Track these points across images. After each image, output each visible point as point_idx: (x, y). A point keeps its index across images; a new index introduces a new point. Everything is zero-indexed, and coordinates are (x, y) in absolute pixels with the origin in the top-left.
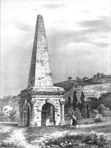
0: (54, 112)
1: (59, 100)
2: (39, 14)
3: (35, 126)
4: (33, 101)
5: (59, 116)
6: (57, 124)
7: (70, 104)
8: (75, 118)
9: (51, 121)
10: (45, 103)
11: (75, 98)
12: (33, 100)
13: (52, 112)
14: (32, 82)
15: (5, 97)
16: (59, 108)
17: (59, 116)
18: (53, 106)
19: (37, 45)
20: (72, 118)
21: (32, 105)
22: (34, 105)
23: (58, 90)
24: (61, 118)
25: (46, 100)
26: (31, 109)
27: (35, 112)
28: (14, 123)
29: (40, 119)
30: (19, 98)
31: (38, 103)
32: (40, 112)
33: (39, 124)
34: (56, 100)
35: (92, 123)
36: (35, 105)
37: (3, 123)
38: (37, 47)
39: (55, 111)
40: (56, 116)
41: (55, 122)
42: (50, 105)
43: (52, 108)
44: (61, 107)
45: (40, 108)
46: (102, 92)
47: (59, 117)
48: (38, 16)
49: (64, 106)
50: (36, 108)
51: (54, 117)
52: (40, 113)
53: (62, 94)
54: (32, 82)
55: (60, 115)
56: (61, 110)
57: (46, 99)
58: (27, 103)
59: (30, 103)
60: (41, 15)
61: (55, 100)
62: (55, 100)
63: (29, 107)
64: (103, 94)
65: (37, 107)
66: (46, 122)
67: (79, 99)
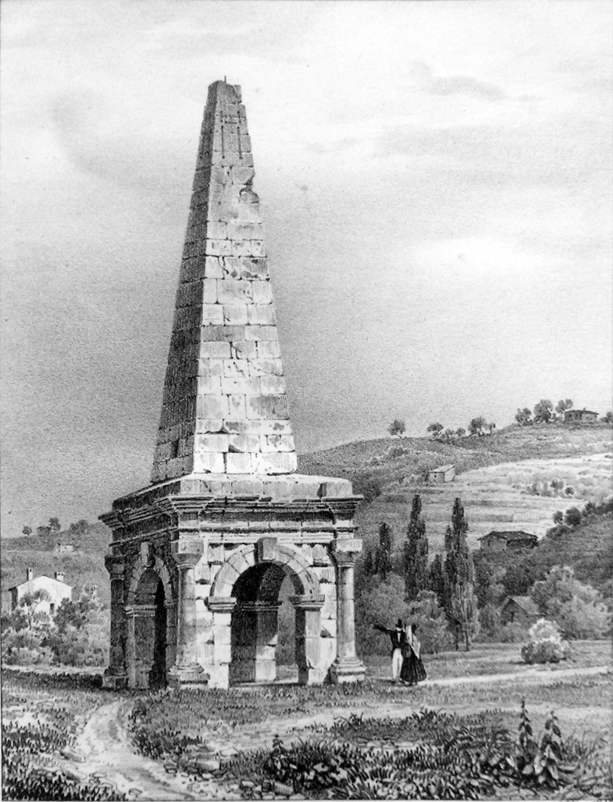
0: (300, 615)
1: (330, 547)
2: (223, 80)
3: (201, 686)
6: (316, 677)
7: (416, 519)
8: (416, 645)
9: (280, 660)
10: (294, 611)
11: (417, 530)
12: (184, 543)
13: (286, 612)
14: (176, 446)
15: (26, 531)
16: (328, 589)
17: (324, 635)
18: (295, 576)
20: (403, 645)
21: (178, 576)
22: (190, 573)
23: (320, 494)
24: (341, 642)
25: (258, 548)
26: (175, 595)
27: (196, 612)
28: (69, 670)
29: (224, 651)
30: (106, 538)
32: (227, 611)
33: (220, 679)
36: (193, 575)
37: (175, 660)
39: (305, 609)
40: (311, 636)
41: (304, 670)
42: (278, 571)
43: (286, 590)
44: (339, 583)
45: (225, 592)
46: (565, 505)
47: (327, 640)
48: (213, 89)
49: (355, 576)
50: (203, 591)
51: (301, 642)
52: (227, 618)
53: (349, 516)
54: (176, 446)
57: (254, 538)
58: (153, 564)
59: (171, 563)
60: (228, 82)
61: (300, 545)
63: (161, 586)
64: (568, 512)
66: (255, 659)
67: (436, 540)
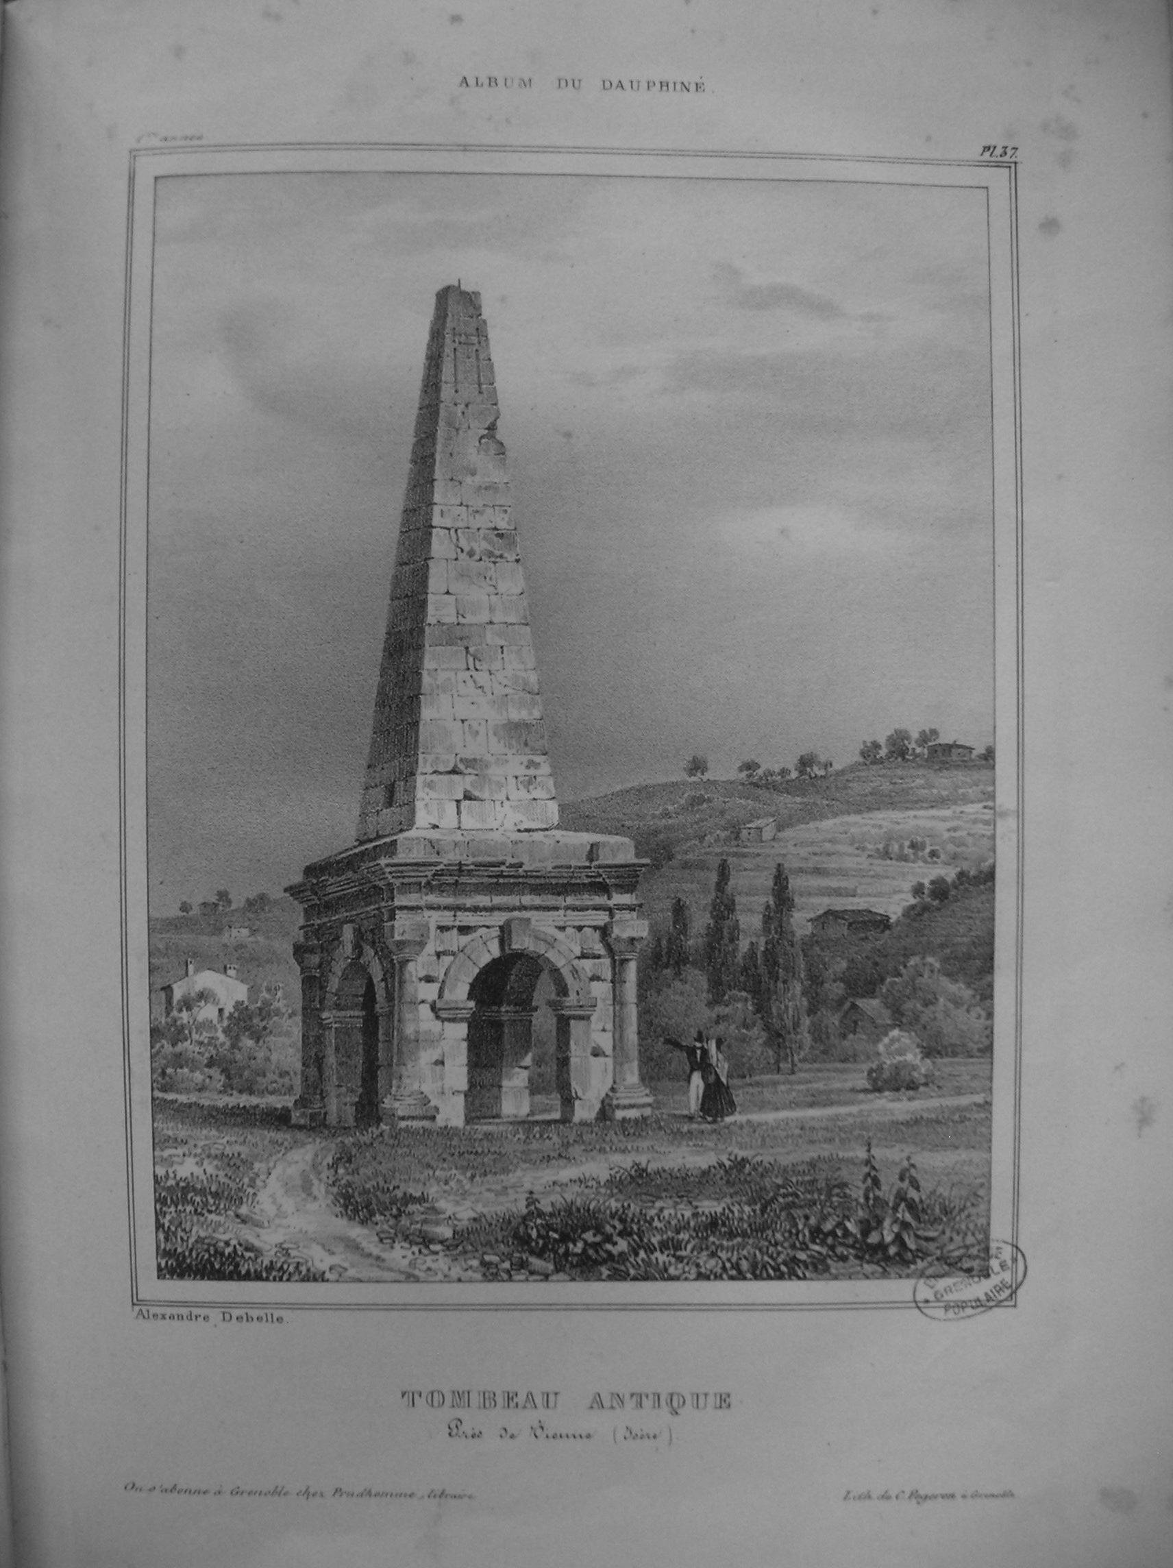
0: (563, 1024)
1: (604, 931)
2: (456, 284)
3: (426, 1124)
4: (397, 938)
5: (597, 1053)
6: (584, 1111)
7: (723, 892)
9: (535, 1088)
11: (724, 908)
12: (403, 926)
13: (543, 1021)
14: (391, 790)
15: (185, 907)
16: (601, 990)
17: (597, 1053)
19: (437, 510)
20: (704, 1065)
21: (394, 971)
22: (411, 966)
25: (505, 933)
28: (245, 1100)
29: (457, 1074)
30: (294, 918)
31: (438, 955)
32: (461, 1020)
33: (453, 1113)
34: (580, 928)
35: (794, 1104)
36: (415, 969)
38: (436, 520)
40: (577, 1054)
41: (568, 1101)
42: (532, 965)
43: (544, 991)
44: (617, 981)
45: (460, 993)
46: (927, 873)
47: (601, 1059)
48: (444, 296)
49: (639, 971)
50: (429, 992)
53: (629, 888)
54: (391, 790)
55: (608, 1049)
56: (618, 1000)
57: (499, 918)
58: (360, 955)
62: (562, 928)
63: (370, 985)
65: (429, 979)
66: (500, 1087)
67: (750, 921)
